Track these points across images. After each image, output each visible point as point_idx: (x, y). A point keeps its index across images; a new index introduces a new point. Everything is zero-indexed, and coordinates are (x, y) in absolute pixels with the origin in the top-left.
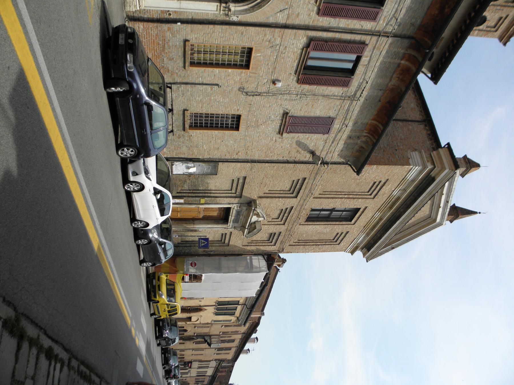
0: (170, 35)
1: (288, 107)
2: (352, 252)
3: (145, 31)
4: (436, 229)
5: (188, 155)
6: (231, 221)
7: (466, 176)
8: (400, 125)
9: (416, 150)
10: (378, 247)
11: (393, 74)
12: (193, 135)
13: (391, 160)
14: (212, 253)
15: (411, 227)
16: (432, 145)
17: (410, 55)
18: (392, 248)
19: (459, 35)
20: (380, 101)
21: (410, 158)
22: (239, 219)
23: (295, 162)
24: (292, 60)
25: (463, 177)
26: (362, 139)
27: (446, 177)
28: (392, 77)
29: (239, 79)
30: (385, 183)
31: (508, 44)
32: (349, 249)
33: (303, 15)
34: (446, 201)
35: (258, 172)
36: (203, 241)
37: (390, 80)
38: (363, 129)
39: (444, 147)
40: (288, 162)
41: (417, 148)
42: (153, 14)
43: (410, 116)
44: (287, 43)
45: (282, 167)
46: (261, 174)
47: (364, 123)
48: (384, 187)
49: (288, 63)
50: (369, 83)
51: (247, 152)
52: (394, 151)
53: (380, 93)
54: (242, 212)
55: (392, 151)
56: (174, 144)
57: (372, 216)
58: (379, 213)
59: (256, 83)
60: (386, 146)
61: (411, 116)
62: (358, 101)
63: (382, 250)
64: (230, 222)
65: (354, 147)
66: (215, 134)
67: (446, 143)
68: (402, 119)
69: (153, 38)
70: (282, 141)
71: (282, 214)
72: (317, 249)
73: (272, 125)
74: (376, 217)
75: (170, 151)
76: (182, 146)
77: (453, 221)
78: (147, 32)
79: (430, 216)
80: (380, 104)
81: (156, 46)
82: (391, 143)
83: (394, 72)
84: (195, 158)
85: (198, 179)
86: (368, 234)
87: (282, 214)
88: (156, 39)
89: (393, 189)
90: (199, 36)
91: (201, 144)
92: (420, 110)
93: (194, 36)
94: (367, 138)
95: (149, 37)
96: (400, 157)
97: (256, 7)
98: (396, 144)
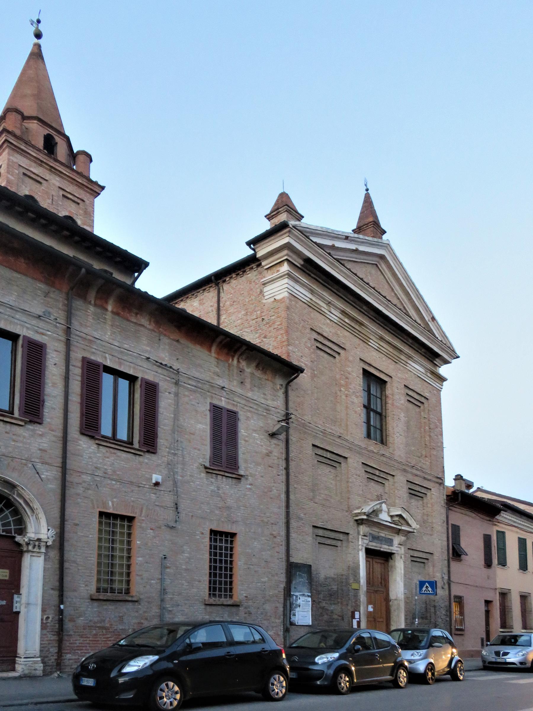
0: (82, 619)
1: (194, 467)
2: (442, 379)
3: (76, 651)
4: (398, 254)
5: (279, 603)
6: (389, 549)
7: (300, 212)
8: (226, 318)
9: (261, 292)
10: (432, 342)
11: (132, 322)
12: (244, 595)
13: (279, 325)
14: (446, 577)
15: (396, 294)
16: (252, 268)
17: (96, 298)
18: (433, 321)
19: (77, 238)
20: (178, 341)
21: (275, 299)
22: (385, 538)
23: (287, 460)
24: (116, 460)
25: (303, 217)
26: (243, 366)
27: (302, 241)
28: (135, 323)
29: (151, 531)
30: (319, 334)
31: (101, 183)
32: (436, 385)
33: (43, 444)
34: (345, 241)
35: (305, 509)
36: (424, 589)
37: (142, 326)
38: (227, 365)
39: (254, 250)
40: (287, 469)
41: (258, 290)
42: (47, 640)
43: (211, 306)
44: (90, 467)
45: (295, 477)
46: (308, 506)
47: (216, 363)
48: (325, 334)
49: (122, 465)
50: (148, 356)
51: (272, 524)
52: (264, 322)
53: (165, 340)
54: (374, 533)
55: (264, 325)
56: (261, 620)
57: (377, 352)
58: (371, 341)
59: (157, 508)
60: (257, 335)
61: (212, 304)
62: (179, 371)
63: (437, 336)
64: (392, 550)
65: (259, 377)
66: (243, 565)
67: (248, 247)
68: (216, 316)
69: (88, 642)
70: (251, 476)
71: (376, 478)
72: (437, 430)
73: (225, 488)
74: (378, 345)
75: (273, 627)
76: (264, 609)
77: (383, 230)
78: (78, 650)
79: (375, 266)
80: (183, 341)
81: (101, 638)
82: (252, 328)
83: (128, 320)
84: (283, 593)
85: (319, 591)
86: (410, 357)
87: (376, 478)
88: (89, 638)
89: (328, 321)
90: (83, 581)
91: (259, 584)
92: (201, 292)
93: (82, 588)
94: (242, 358)
95: (86, 647)
96: (273, 314)
97: (33, 505)
98: (254, 322)
